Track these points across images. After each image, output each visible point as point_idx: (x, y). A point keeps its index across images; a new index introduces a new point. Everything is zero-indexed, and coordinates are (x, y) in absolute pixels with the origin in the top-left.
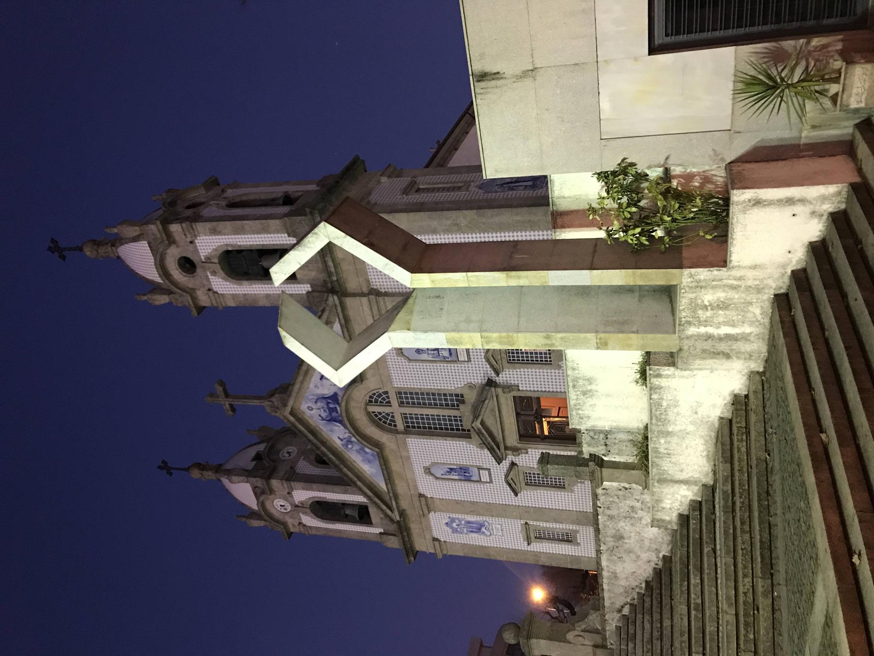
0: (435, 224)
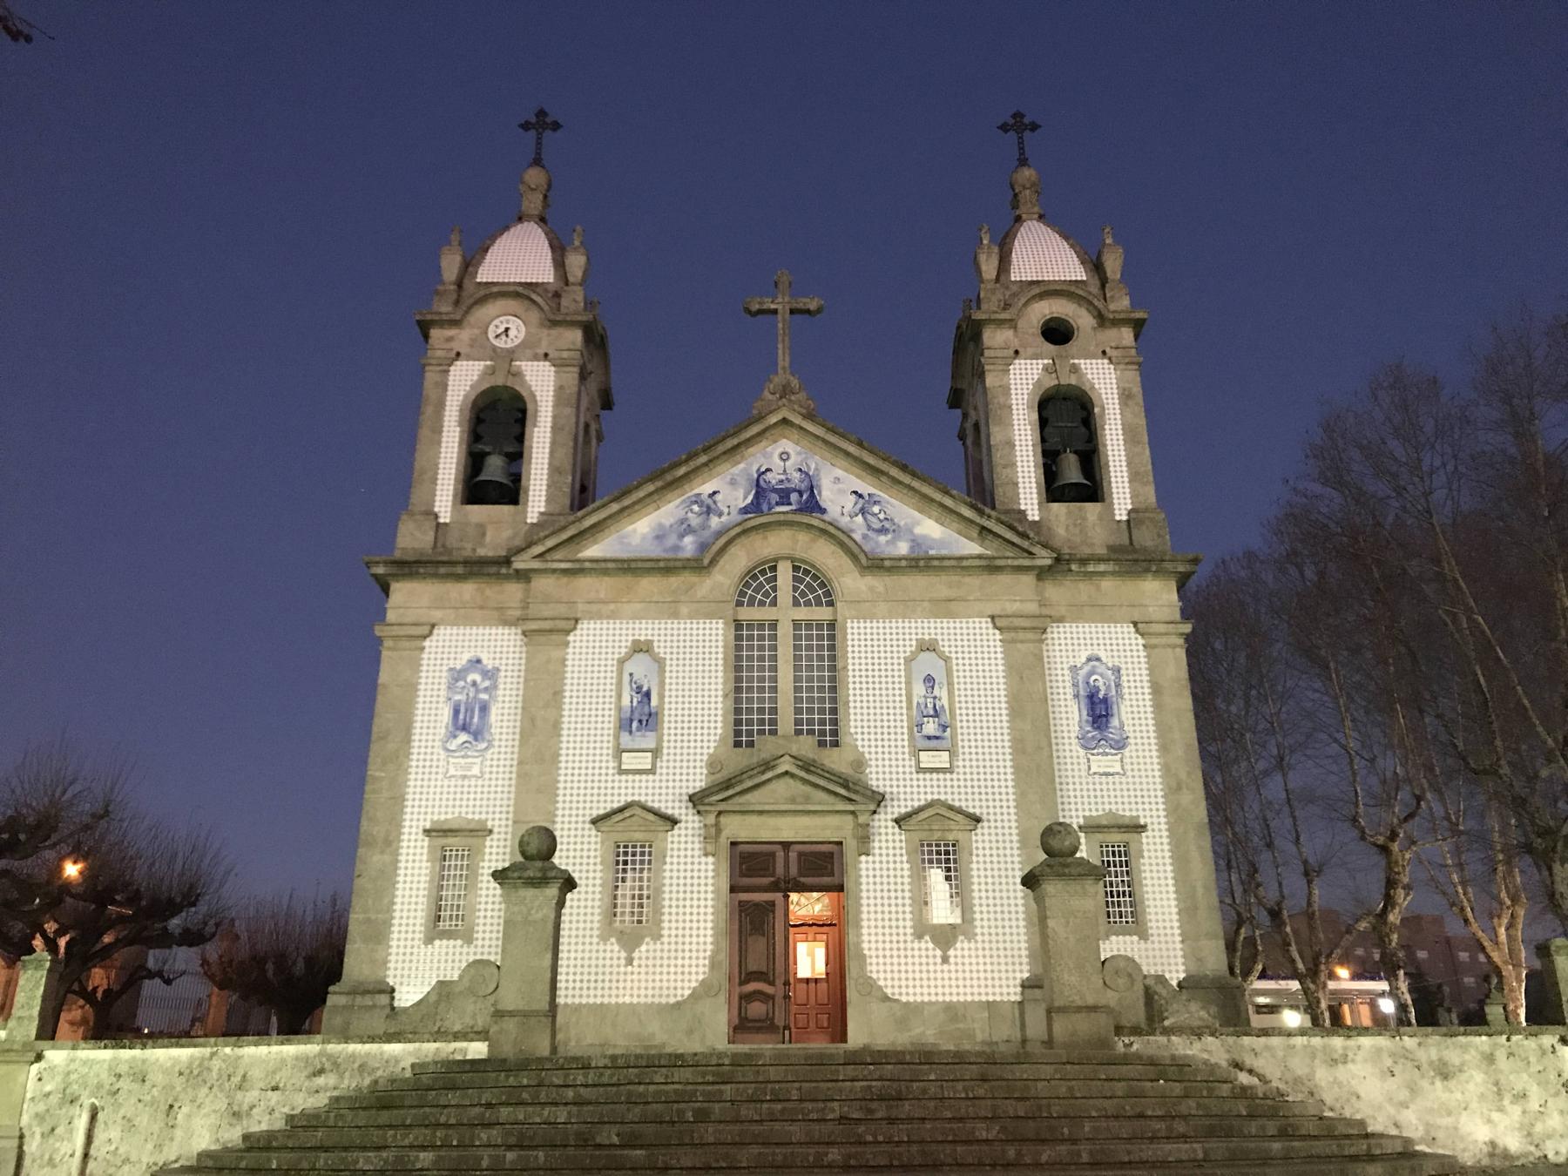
0: (1179, 751)
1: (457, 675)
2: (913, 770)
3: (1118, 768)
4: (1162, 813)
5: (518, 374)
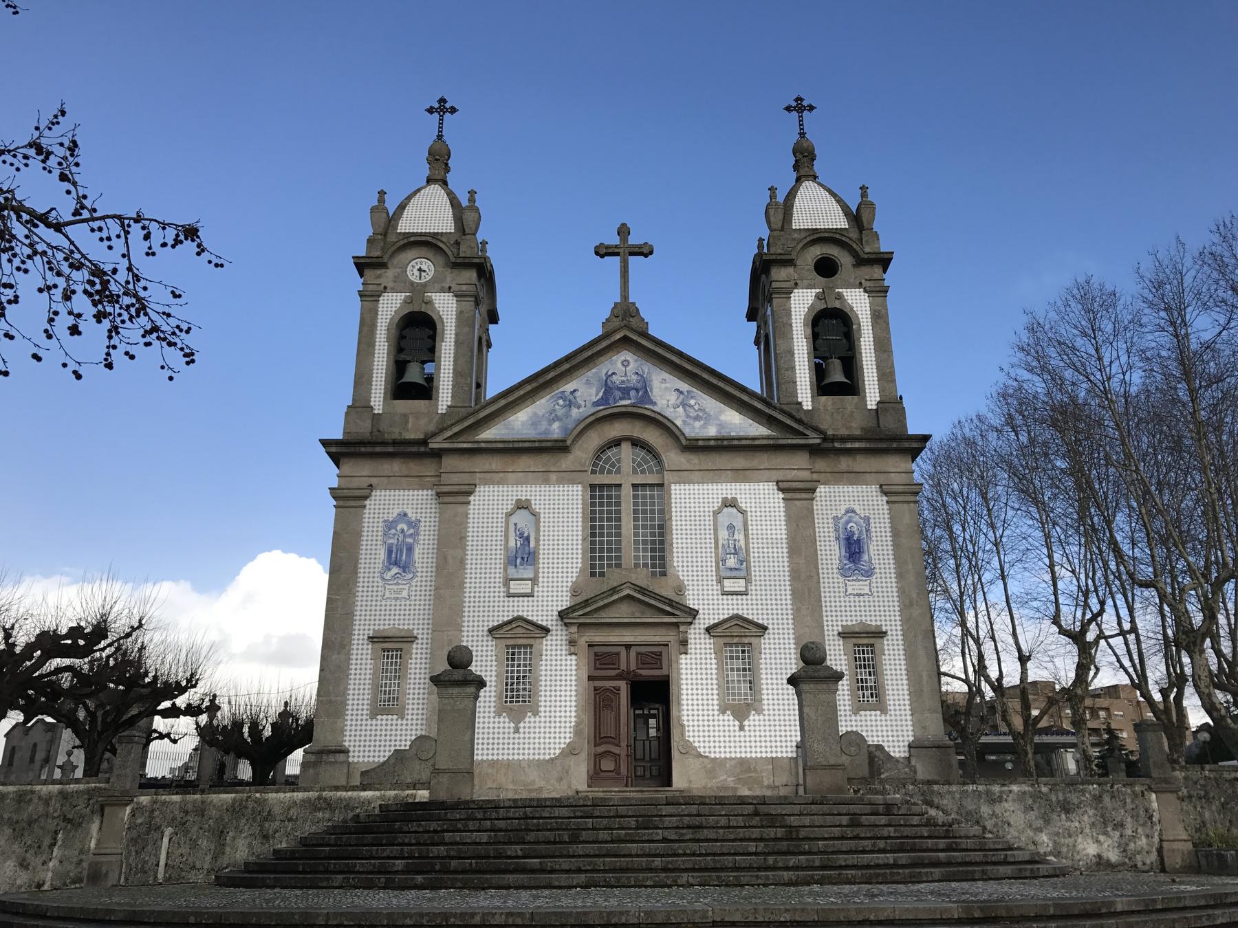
1: (390, 525)
2: (719, 592)
3: (867, 590)
4: (899, 623)
5: (429, 303)
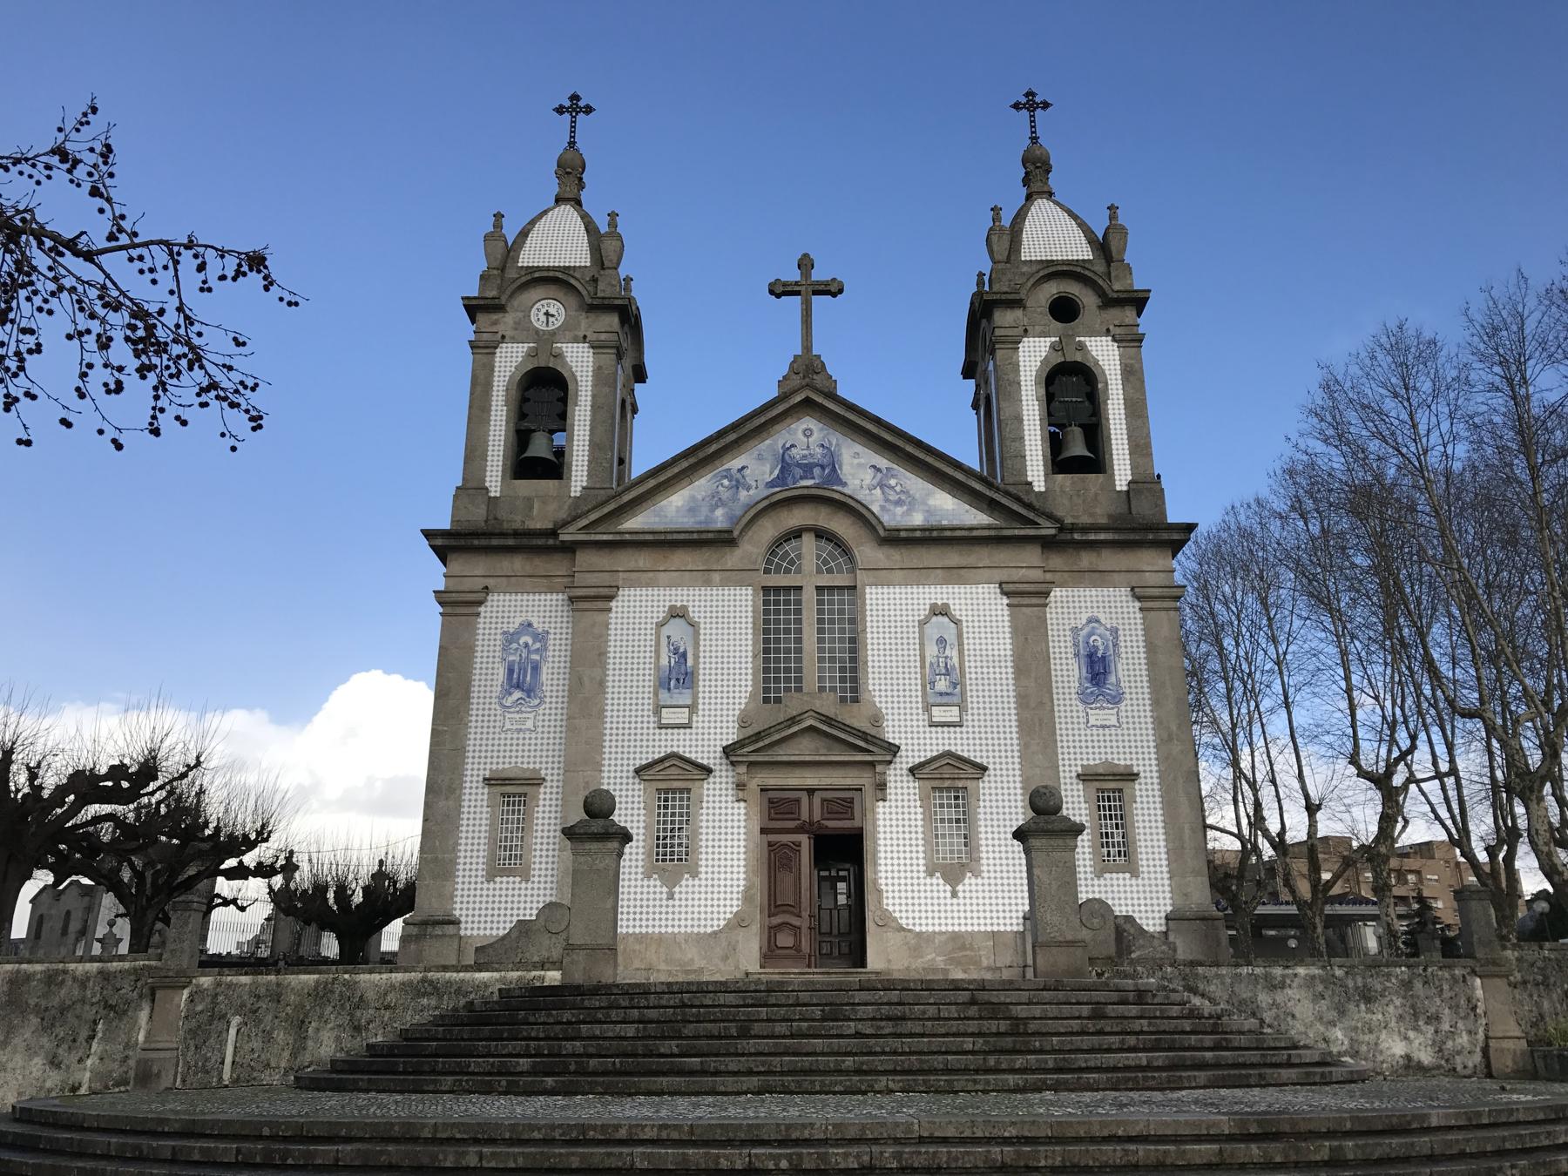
1: (510, 638)
2: (926, 723)
3: (1113, 721)
4: (1154, 762)
5: (559, 356)
